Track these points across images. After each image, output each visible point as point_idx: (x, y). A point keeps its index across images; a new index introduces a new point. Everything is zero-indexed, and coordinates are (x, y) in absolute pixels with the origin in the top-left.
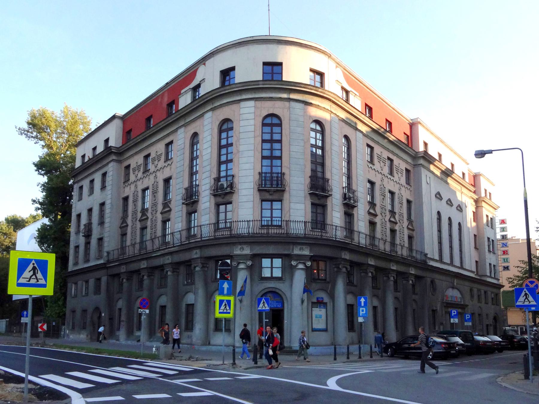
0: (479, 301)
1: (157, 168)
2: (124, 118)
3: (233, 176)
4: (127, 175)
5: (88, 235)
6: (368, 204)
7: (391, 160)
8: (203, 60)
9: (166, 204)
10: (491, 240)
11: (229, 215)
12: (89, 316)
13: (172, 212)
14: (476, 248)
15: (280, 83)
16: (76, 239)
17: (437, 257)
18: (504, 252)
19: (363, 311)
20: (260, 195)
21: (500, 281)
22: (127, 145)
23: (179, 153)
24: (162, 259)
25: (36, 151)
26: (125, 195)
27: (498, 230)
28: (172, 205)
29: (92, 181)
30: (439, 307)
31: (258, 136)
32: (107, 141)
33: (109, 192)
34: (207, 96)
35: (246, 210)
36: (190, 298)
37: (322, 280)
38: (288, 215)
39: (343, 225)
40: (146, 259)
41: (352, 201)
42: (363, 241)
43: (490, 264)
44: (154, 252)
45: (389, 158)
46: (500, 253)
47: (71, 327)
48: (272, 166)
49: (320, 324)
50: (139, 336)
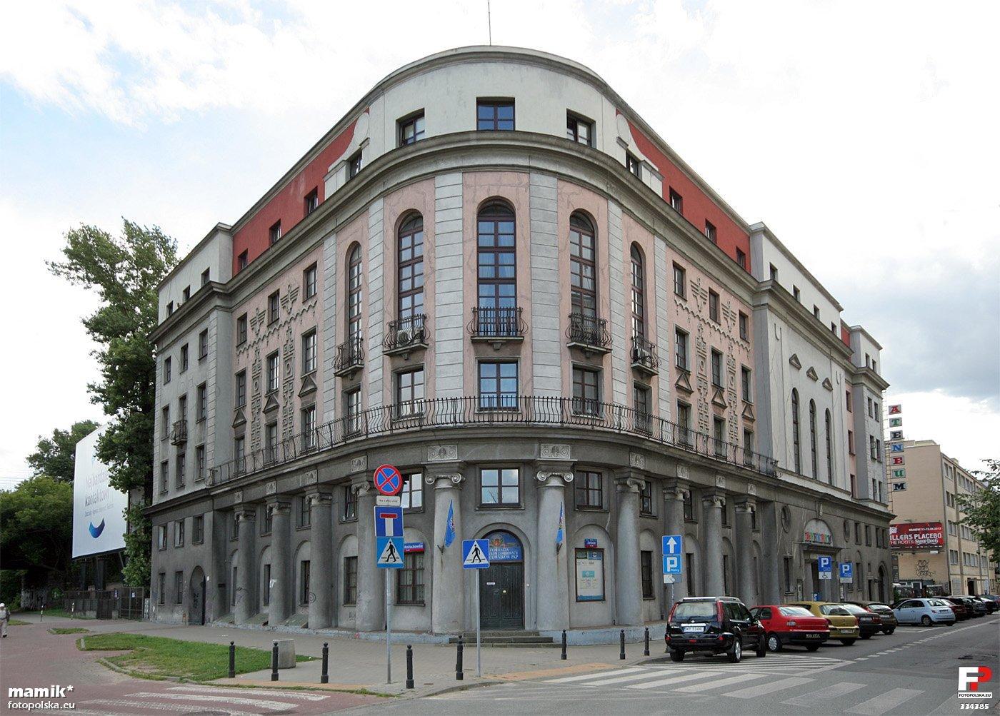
0: (858, 542)
1: (291, 315)
2: (233, 232)
3: (425, 317)
4: (243, 333)
5: (181, 444)
6: (675, 371)
7: (714, 295)
8: (364, 105)
9: (308, 379)
10: (875, 440)
11: (419, 392)
12: (186, 582)
13: (318, 393)
14: (851, 453)
15: (510, 135)
16: (163, 451)
17: (792, 468)
18: (896, 459)
19: (672, 562)
20: (477, 352)
21: (889, 508)
22: (241, 276)
23: (327, 284)
24: (300, 477)
25: (92, 300)
26: (240, 369)
27: (886, 424)
28: (318, 381)
29: (185, 349)
30: (795, 552)
31: (470, 240)
32: (206, 274)
33: (212, 365)
34: (372, 168)
35: (450, 380)
36: (351, 547)
37: (594, 507)
38: (529, 388)
39: (632, 405)
40: (275, 478)
41: (648, 364)
42: (668, 438)
43: (874, 480)
44: (287, 464)
45: (712, 293)
46: (889, 461)
47: (159, 601)
48: (497, 297)
49: (591, 588)
50: (267, 615)
